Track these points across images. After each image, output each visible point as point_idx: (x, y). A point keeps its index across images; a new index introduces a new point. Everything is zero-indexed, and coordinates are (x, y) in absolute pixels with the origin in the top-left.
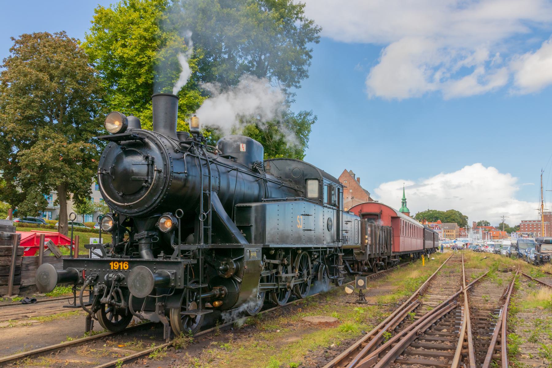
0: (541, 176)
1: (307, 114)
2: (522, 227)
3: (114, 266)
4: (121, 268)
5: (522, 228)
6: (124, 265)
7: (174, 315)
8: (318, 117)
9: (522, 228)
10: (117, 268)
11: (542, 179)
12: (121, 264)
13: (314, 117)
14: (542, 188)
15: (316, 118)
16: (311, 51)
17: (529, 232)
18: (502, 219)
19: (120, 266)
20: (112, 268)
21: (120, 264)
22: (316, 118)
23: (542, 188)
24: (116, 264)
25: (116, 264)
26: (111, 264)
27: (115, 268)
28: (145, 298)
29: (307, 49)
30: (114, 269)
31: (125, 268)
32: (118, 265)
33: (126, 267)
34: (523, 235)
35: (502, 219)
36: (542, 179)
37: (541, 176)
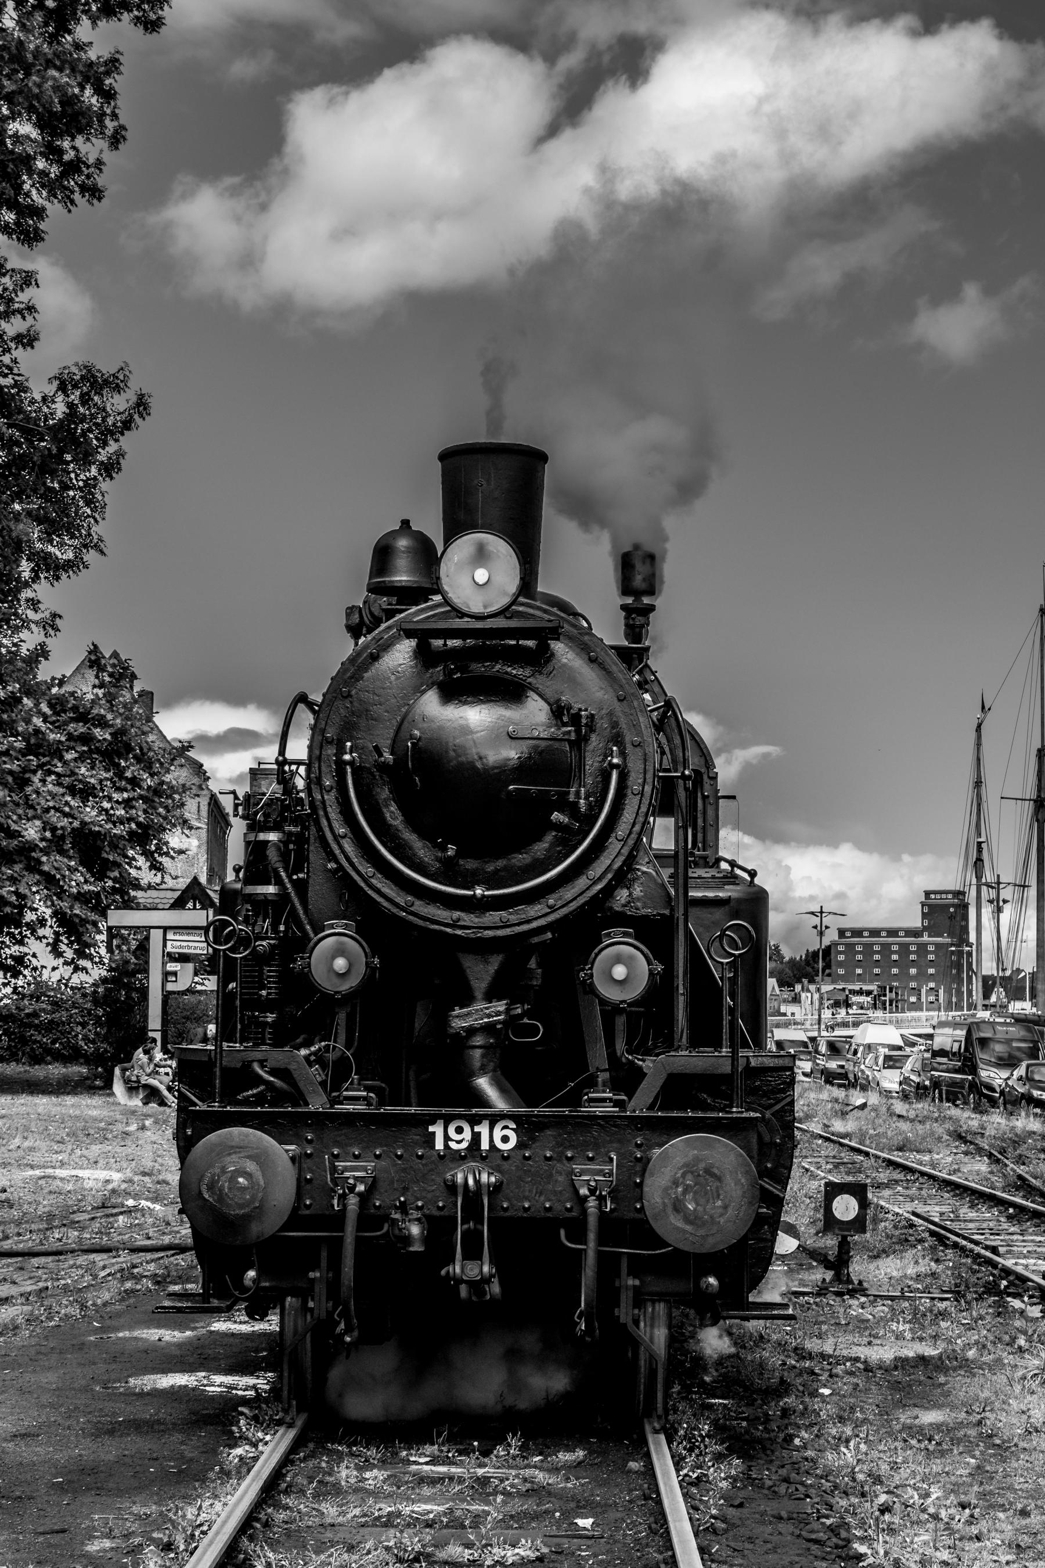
0: (979, 726)
1: (115, 384)
2: (841, 958)
3: (447, 1138)
4: (485, 1145)
5: (840, 964)
6: (498, 1133)
7: (652, 1326)
8: (153, 402)
9: (840, 964)
10: (464, 1145)
11: (979, 744)
12: (483, 1129)
13: (134, 399)
14: (978, 784)
15: (142, 405)
16: (113, 64)
17: (871, 982)
18: (816, 921)
19: (476, 1137)
20: (439, 1145)
21: (477, 1129)
22: (142, 405)
23: (978, 784)
24: (459, 1130)
25: (459, 1130)
26: (437, 1129)
27: (453, 1145)
28: (670, 1245)
29: (92, 55)
30: (446, 1146)
31: (500, 1145)
32: (467, 1135)
33: (505, 1139)
34: (855, 999)
35: (816, 921)
36: (979, 744)
37: (979, 726)
